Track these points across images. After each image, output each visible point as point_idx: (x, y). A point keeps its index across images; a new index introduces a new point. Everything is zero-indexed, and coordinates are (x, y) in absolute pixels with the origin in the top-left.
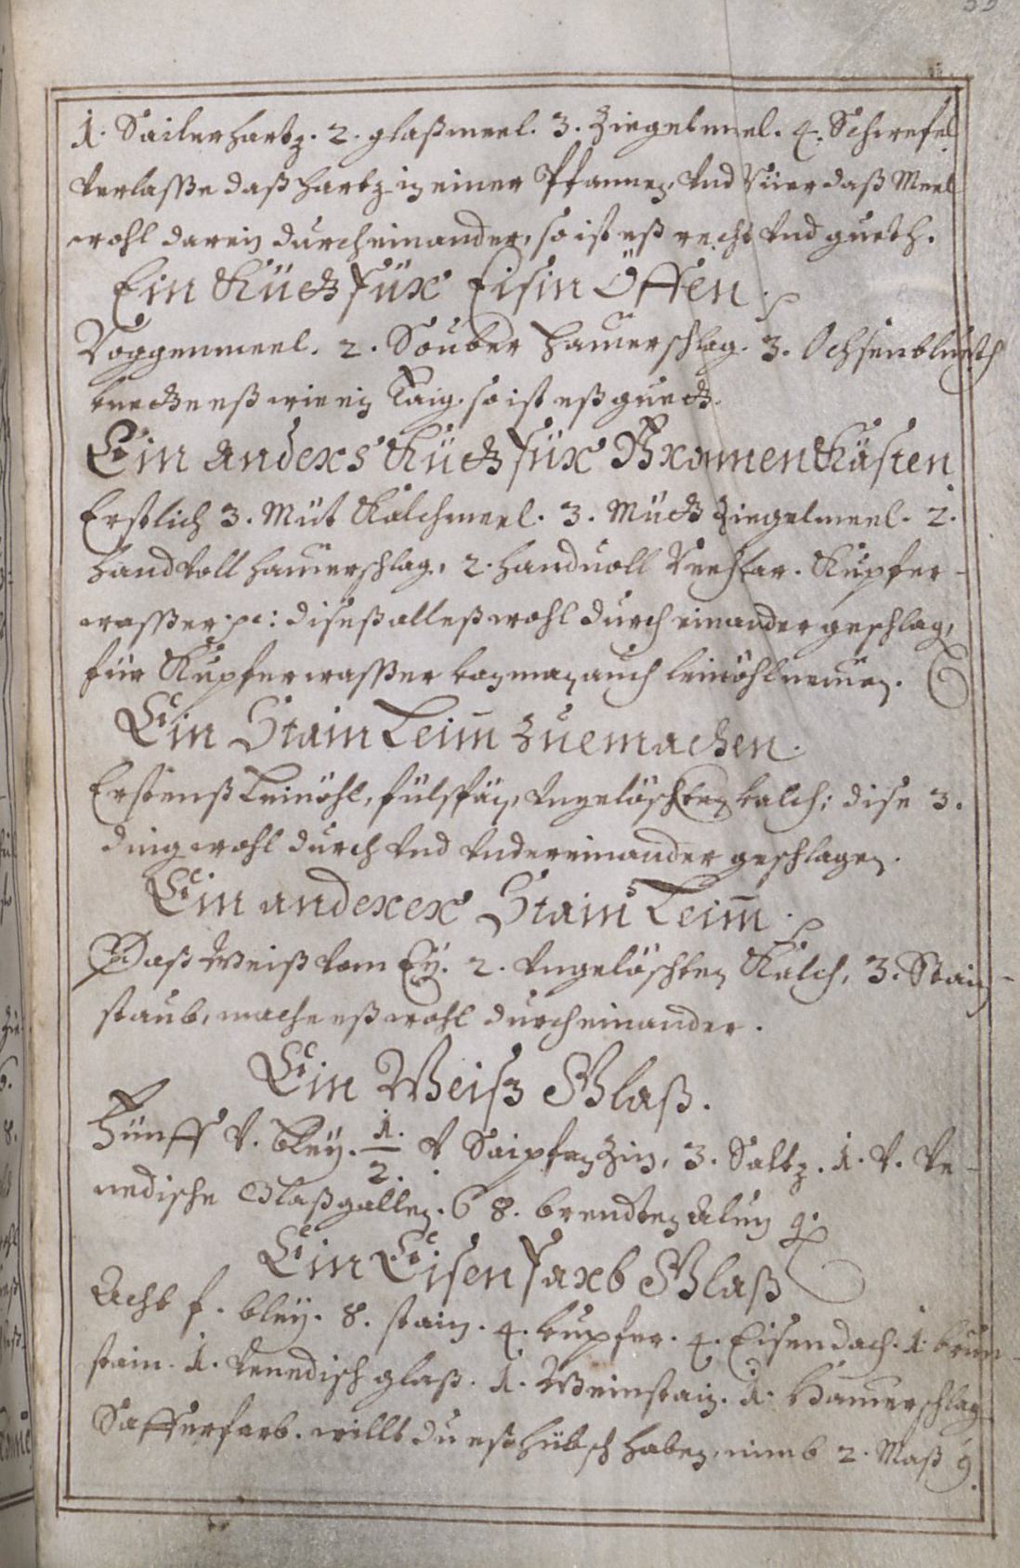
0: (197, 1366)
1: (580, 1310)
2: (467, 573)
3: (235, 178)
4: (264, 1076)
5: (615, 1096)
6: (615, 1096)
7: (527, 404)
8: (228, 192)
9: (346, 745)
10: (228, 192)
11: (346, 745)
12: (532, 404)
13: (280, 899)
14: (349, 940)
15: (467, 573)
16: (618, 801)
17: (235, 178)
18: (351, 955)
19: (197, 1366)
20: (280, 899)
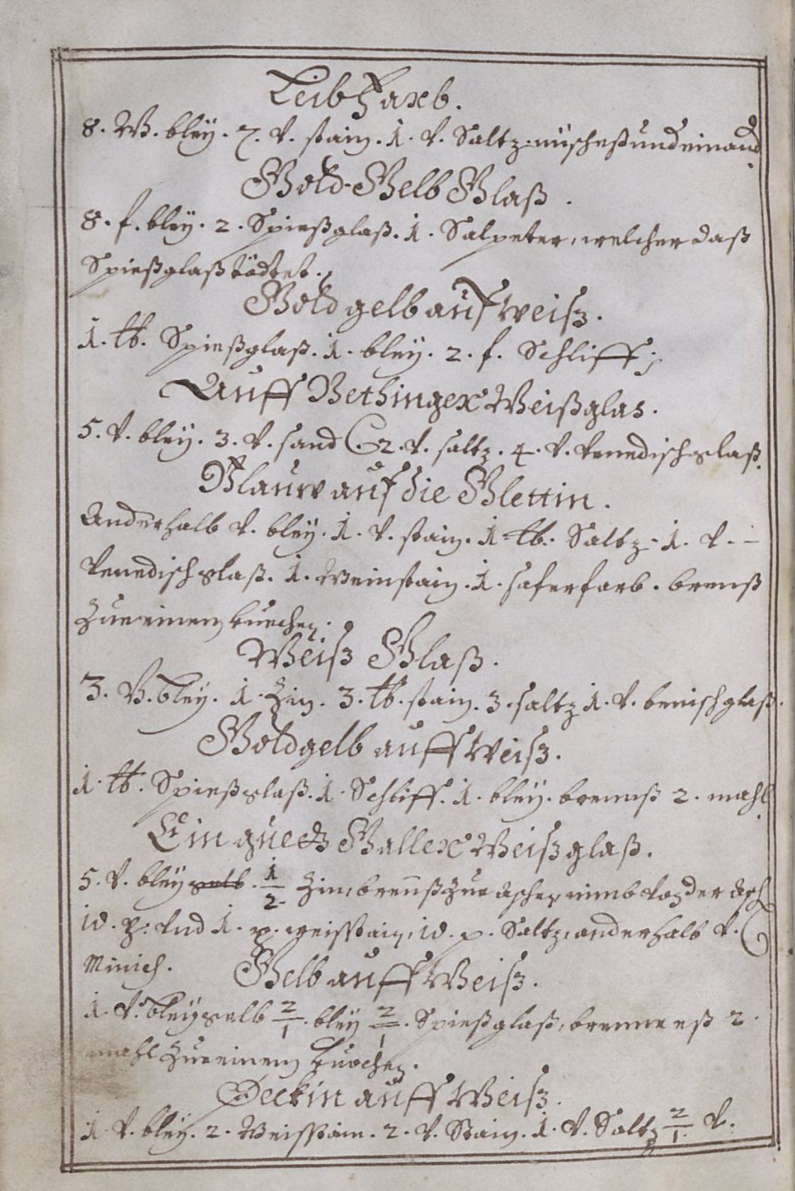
0: (293, 578)
1: (345, 1045)
2: (202, 489)
3: (705, 229)
4: (287, 83)
5: (502, 497)
6: (502, 497)
7: (405, 539)
8: (697, 241)
9: (571, 506)
10: (697, 241)
11: (571, 506)
12: (410, 539)
13: (388, 746)
14: (282, 252)
15: (202, 489)
16: (512, 1027)
17: (705, 229)
18: (589, 790)
19: (293, 578)
20: (388, 746)
